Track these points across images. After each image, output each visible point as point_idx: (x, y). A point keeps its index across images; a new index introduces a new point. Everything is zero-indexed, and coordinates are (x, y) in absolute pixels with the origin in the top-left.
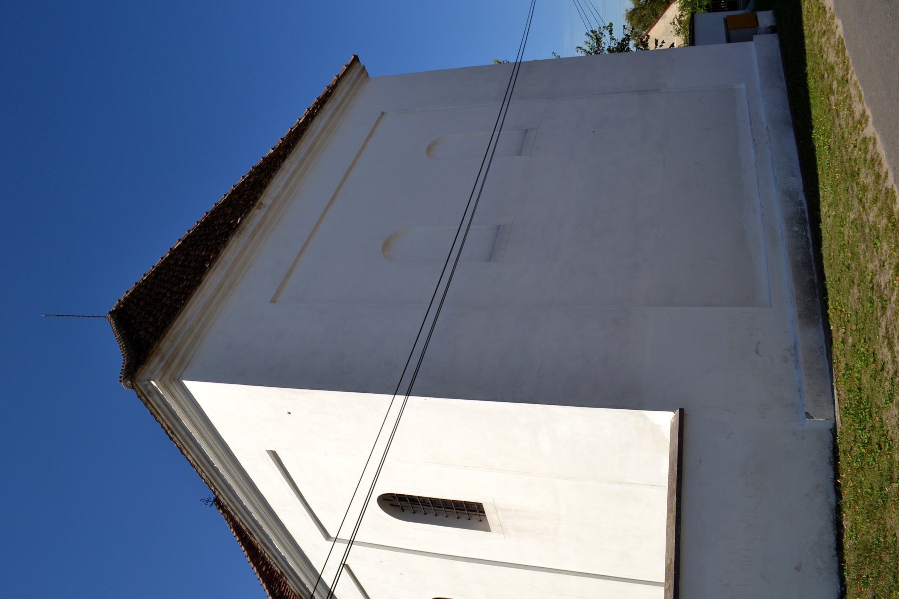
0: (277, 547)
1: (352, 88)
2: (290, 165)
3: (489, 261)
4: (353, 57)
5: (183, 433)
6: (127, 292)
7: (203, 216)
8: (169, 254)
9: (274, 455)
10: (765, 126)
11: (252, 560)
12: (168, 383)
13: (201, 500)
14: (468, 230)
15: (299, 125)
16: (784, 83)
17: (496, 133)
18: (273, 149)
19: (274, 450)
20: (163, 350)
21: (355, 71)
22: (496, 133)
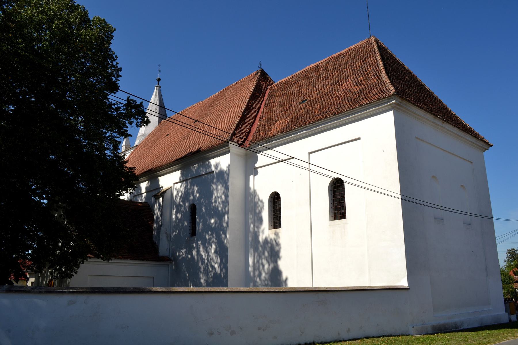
0: (303, 132)
1: (480, 146)
2: (456, 130)
3: (434, 218)
4: (492, 145)
5: (368, 107)
6: (383, 44)
7: (419, 79)
8: (401, 63)
9: (359, 139)
10: (480, 316)
11: (251, 97)
12: (392, 105)
13: (260, 62)
14: (441, 209)
15: (461, 122)
16: (493, 324)
17: (469, 214)
18: (450, 110)
19: (361, 139)
20: (403, 102)
21: (485, 146)
22: (469, 214)
